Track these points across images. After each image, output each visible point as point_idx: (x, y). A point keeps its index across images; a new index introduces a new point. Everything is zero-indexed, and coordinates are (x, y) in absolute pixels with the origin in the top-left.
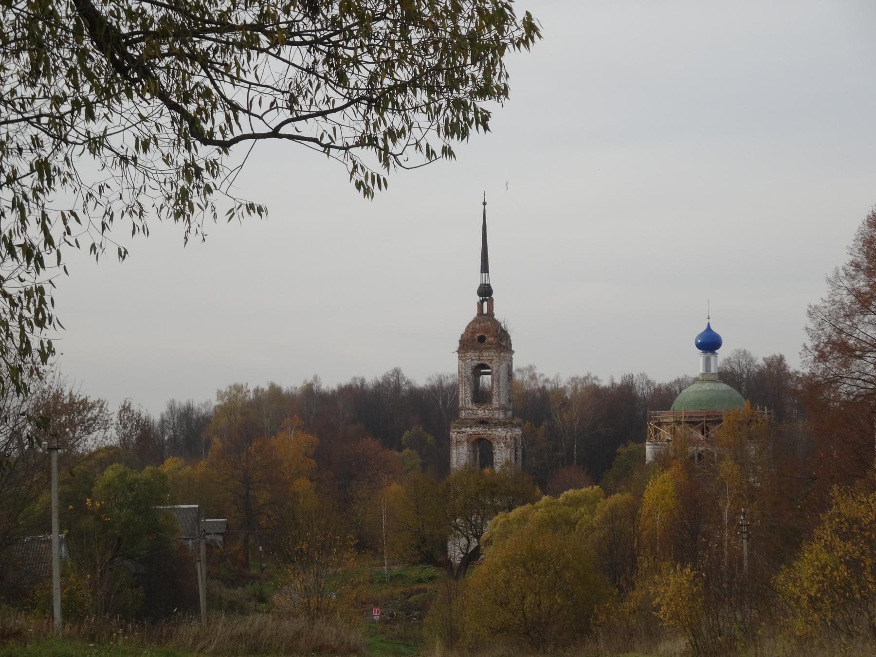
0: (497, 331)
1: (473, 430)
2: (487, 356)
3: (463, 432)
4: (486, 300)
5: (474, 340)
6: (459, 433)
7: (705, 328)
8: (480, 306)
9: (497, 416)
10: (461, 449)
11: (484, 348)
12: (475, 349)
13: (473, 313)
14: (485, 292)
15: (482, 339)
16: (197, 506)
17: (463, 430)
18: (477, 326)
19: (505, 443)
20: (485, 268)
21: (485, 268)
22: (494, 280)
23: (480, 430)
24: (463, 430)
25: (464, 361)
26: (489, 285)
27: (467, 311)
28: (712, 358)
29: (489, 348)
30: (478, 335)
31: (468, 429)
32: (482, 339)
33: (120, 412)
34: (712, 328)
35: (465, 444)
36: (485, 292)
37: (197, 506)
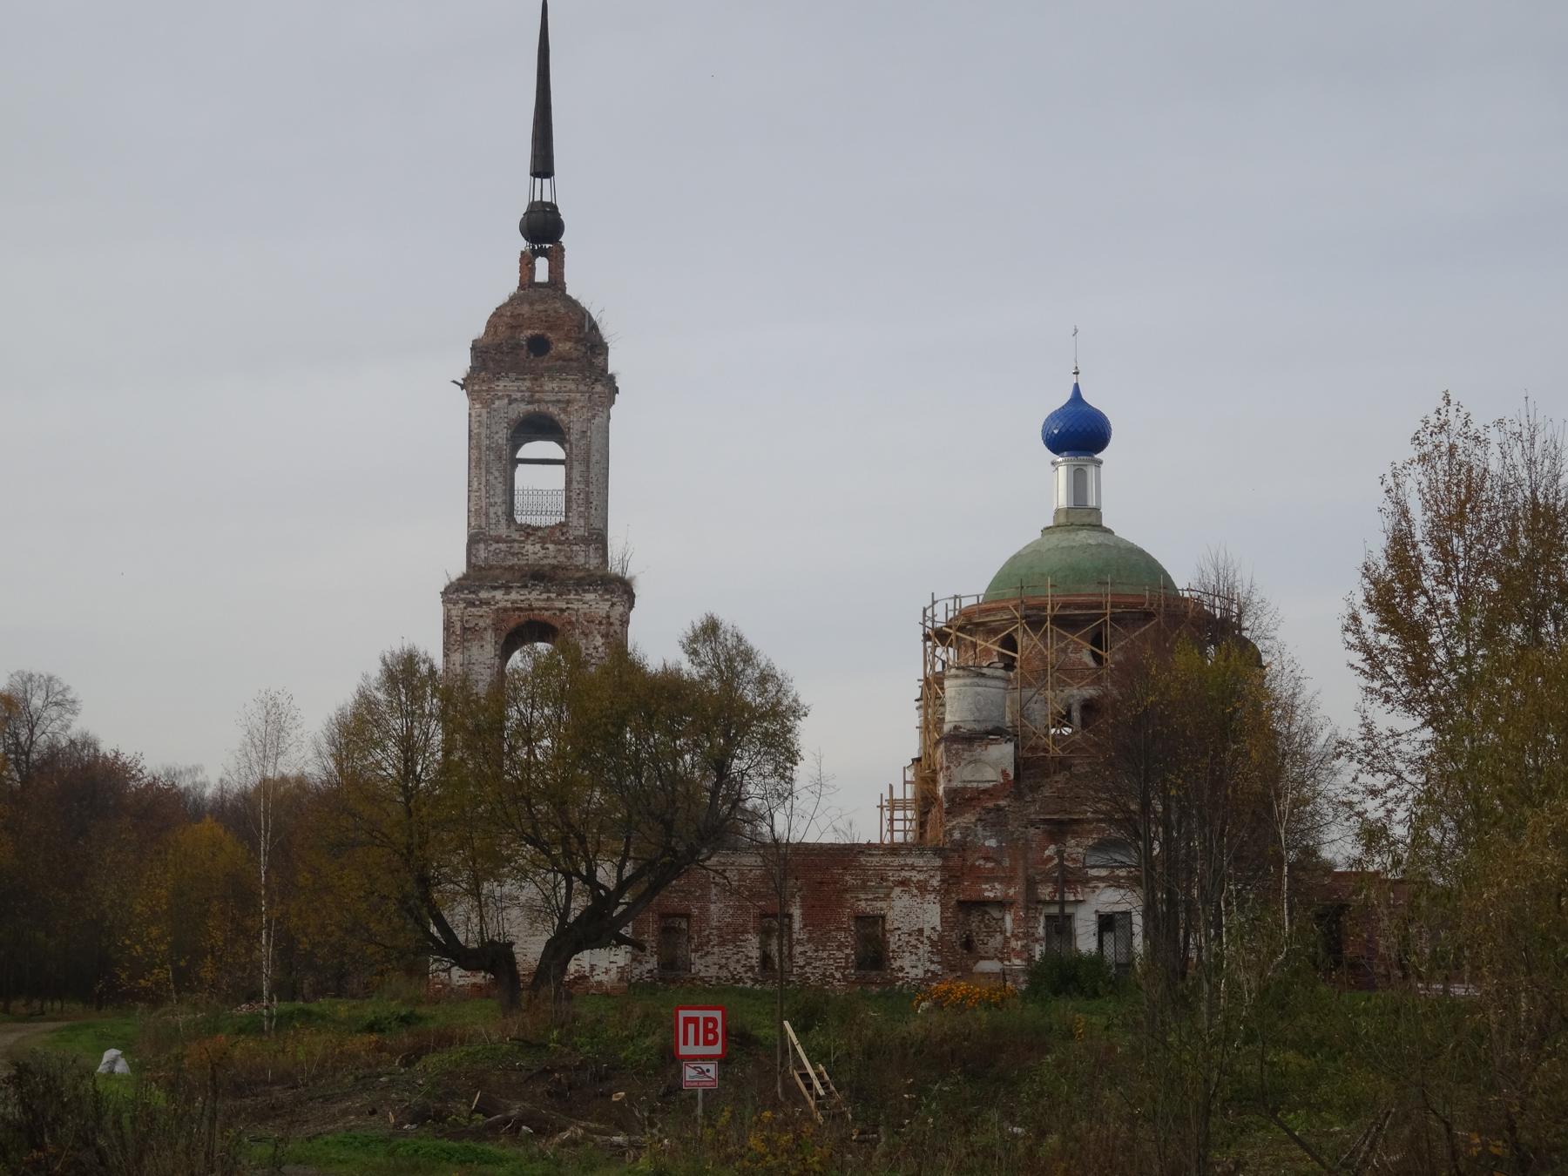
0: (581, 327)
1: (514, 596)
2: (554, 391)
3: (484, 603)
4: (543, 253)
5: (519, 346)
6: (471, 604)
7: (1064, 397)
8: (527, 263)
9: (581, 560)
10: (475, 650)
11: (548, 369)
12: (520, 370)
13: (509, 284)
14: (543, 227)
15: (539, 346)
16: (786, 1023)
17: (483, 595)
18: (525, 309)
19: (605, 636)
20: (543, 166)
21: (543, 166)
22: (565, 192)
23: (535, 597)
24: (483, 595)
25: (487, 404)
26: (554, 208)
27: (493, 274)
28: (1091, 471)
29: (561, 370)
30: (529, 333)
31: (499, 594)
32: (539, 346)
33: (18, 1020)
34: (1086, 396)
35: (489, 636)
36: (543, 227)
37: (786, 1023)
